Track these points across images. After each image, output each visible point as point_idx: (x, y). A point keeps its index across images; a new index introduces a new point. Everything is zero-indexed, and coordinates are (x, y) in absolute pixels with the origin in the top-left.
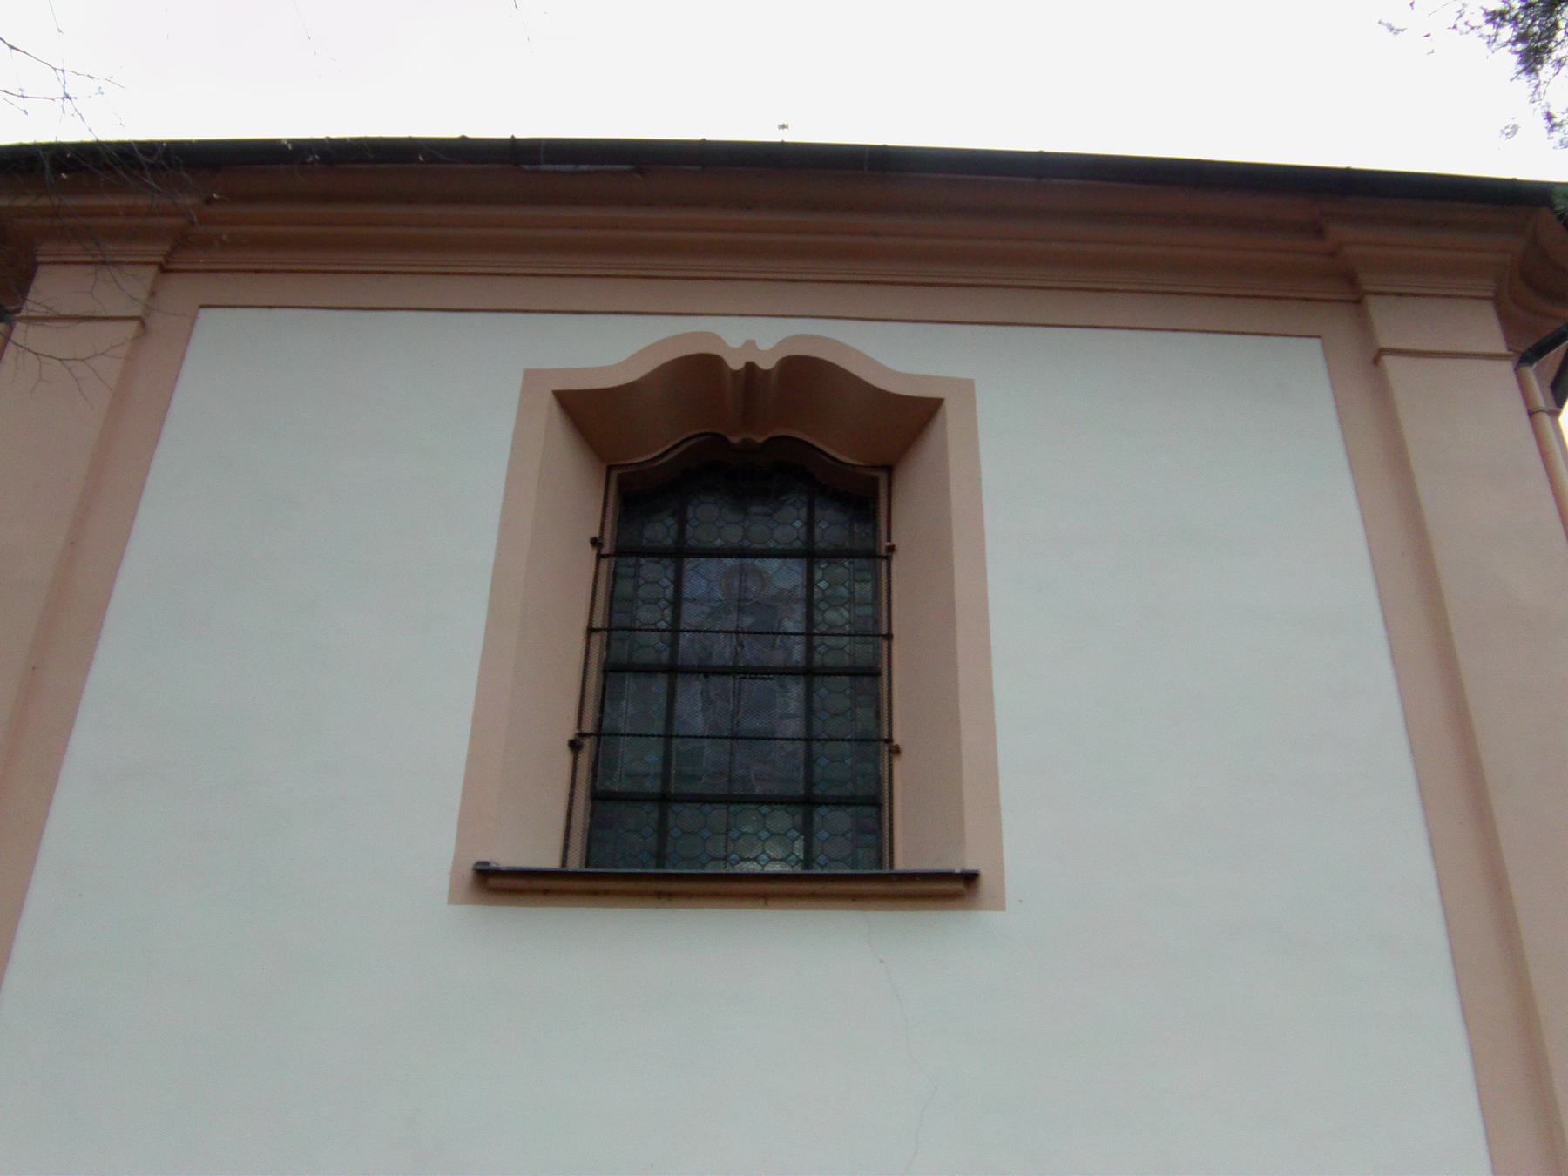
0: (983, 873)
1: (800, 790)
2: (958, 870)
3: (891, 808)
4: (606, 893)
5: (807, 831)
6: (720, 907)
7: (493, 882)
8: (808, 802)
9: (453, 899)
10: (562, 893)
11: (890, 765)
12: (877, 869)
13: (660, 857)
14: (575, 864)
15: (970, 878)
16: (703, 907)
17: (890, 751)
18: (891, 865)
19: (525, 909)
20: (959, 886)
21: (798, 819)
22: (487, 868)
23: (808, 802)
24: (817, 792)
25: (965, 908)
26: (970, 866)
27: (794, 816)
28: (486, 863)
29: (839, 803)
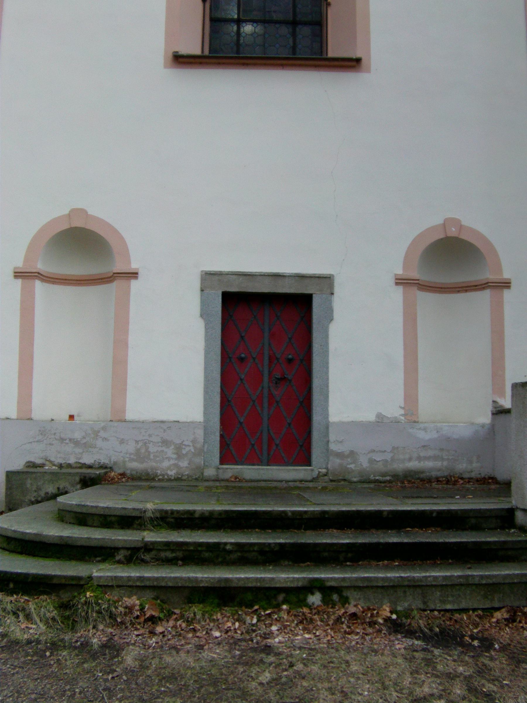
0: (363, 58)
1: (290, 18)
2: (354, 58)
3: (327, 27)
4: (224, 64)
5: (294, 35)
6: (223, 69)
7: (181, 60)
8: (294, 23)
9: (166, 67)
10: (207, 64)
11: (327, 10)
12: (319, 56)
13: (238, 52)
14: (207, 53)
15: (358, 61)
16: (235, 69)
17: (327, 4)
18: (327, 54)
19: (231, 70)
20: (354, 63)
21: (291, 30)
22: (177, 54)
23: (294, 23)
24: (298, 19)
25: (357, 72)
26: (358, 55)
27: (288, 28)
28: (177, 52)
29: (305, 24)
